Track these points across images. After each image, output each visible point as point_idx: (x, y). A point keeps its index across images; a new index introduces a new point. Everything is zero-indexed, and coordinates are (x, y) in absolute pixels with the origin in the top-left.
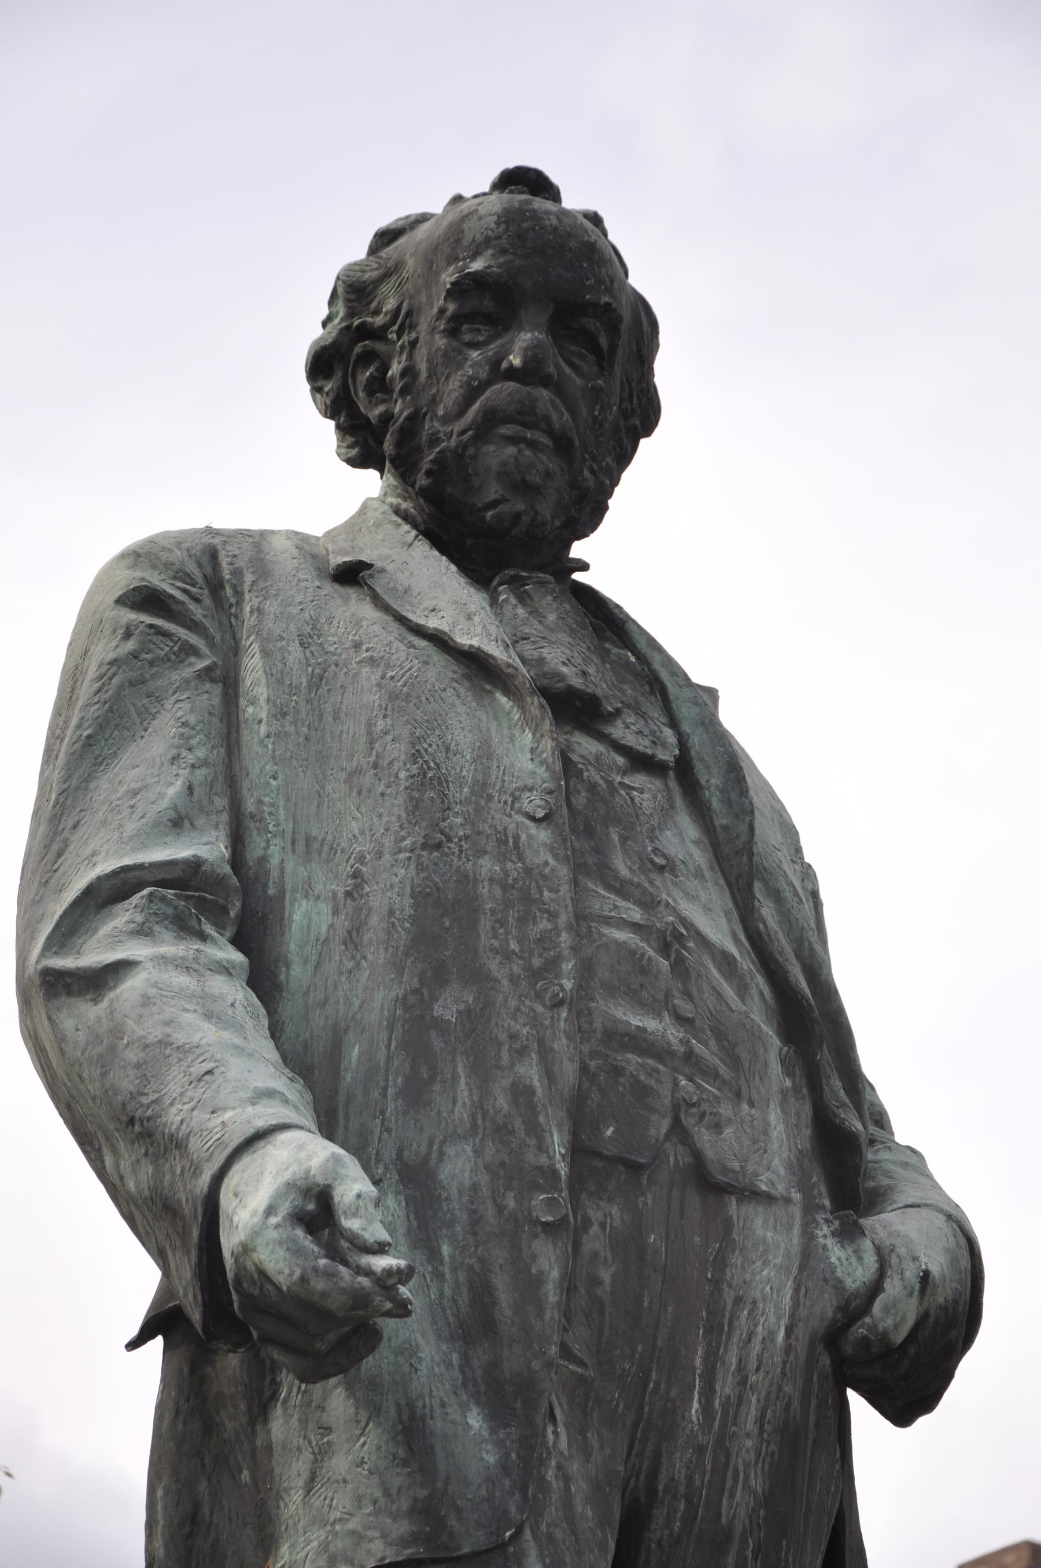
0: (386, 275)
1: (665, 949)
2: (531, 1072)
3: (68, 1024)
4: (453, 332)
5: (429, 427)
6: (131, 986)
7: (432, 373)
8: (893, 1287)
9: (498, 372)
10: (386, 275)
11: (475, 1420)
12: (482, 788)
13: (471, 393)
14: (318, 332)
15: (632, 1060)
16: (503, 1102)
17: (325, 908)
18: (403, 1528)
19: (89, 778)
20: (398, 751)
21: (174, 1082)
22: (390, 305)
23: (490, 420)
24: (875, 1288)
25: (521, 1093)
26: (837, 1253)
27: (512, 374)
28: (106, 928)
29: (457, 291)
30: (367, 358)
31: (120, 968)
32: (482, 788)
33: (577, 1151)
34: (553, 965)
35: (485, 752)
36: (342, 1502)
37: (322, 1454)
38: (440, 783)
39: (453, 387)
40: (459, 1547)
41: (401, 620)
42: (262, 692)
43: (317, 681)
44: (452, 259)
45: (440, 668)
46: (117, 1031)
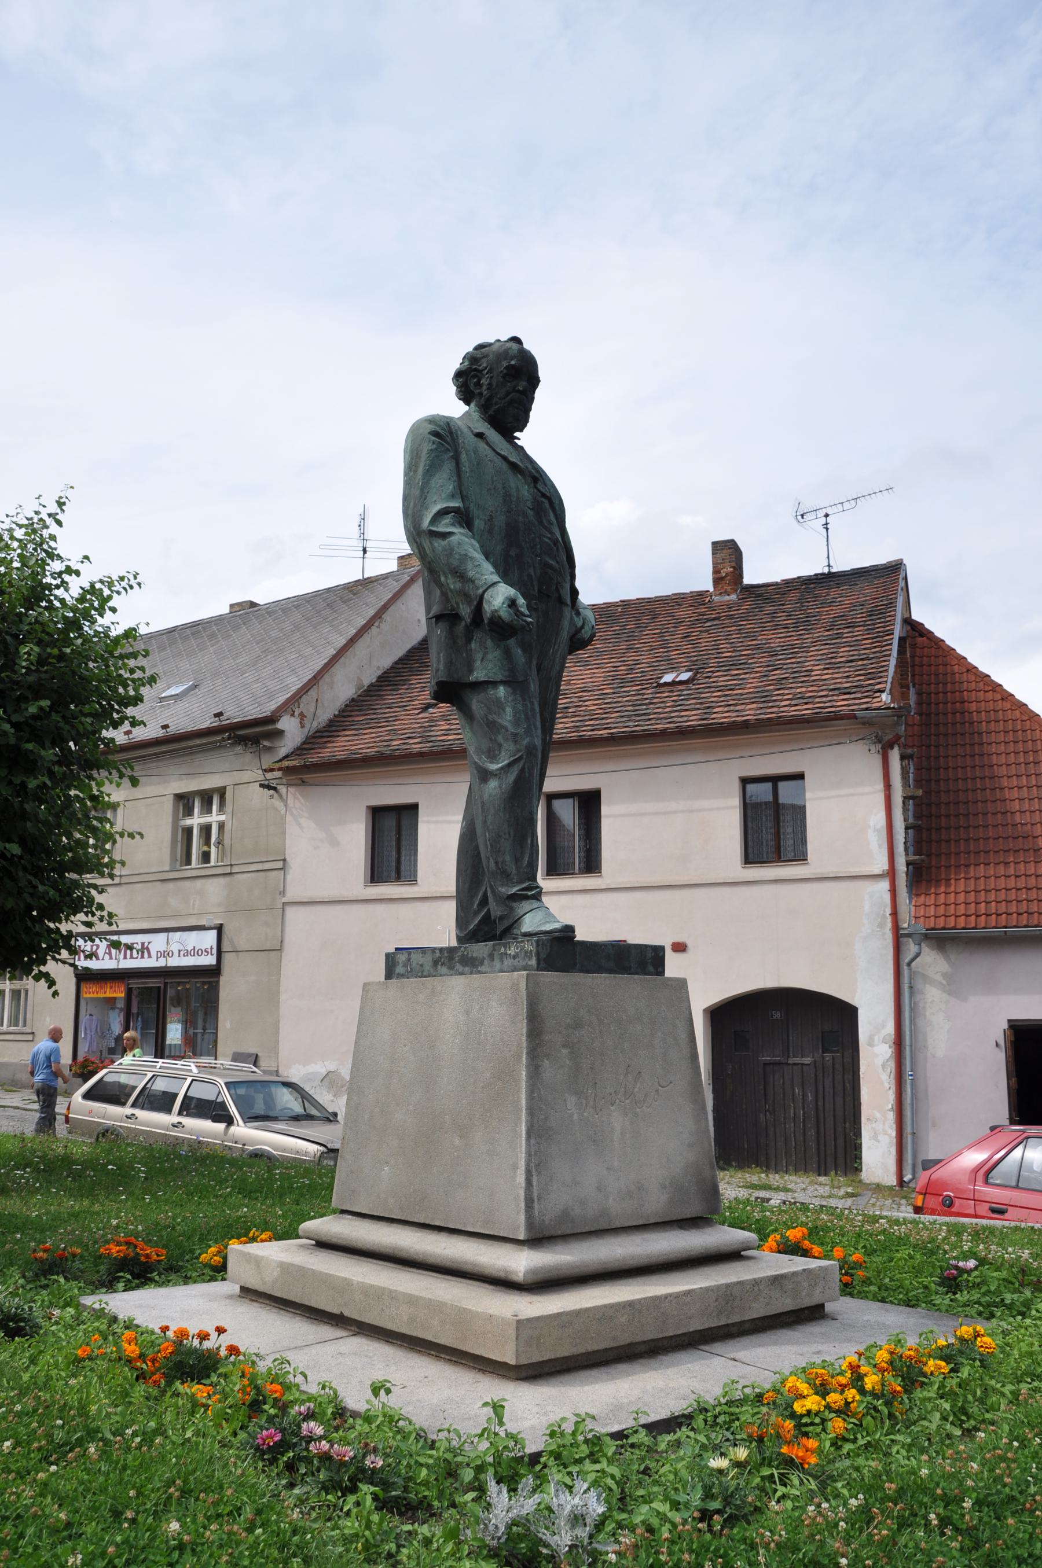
0: (484, 357)
1: (555, 544)
2: (531, 571)
3: (436, 544)
4: (504, 377)
5: (495, 400)
6: (453, 538)
7: (497, 386)
8: (586, 628)
9: (515, 390)
10: (484, 357)
11: (519, 651)
12: (518, 498)
13: (508, 394)
14: (458, 366)
15: (550, 571)
16: (526, 578)
17: (483, 523)
18: (507, 673)
19: (429, 480)
20: (500, 486)
21: (470, 566)
22: (485, 365)
23: (512, 402)
24: (582, 627)
25: (530, 576)
26: (576, 619)
27: (519, 391)
28: (444, 522)
29: (507, 368)
30: (474, 376)
31: (451, 534)
32: (518, 498)
33: (540, 591)
34: (535, 545)
35: (518, 490)
36: (490, 666)
37: (485, 654)
38: (510, 495)
39: (503, 391)
40: (471, 671)
41: (494, 450)
42: (467, 464)
43: (478, 464)
44: (505, 359)
45: (505, 466)
46: (452, 549)
